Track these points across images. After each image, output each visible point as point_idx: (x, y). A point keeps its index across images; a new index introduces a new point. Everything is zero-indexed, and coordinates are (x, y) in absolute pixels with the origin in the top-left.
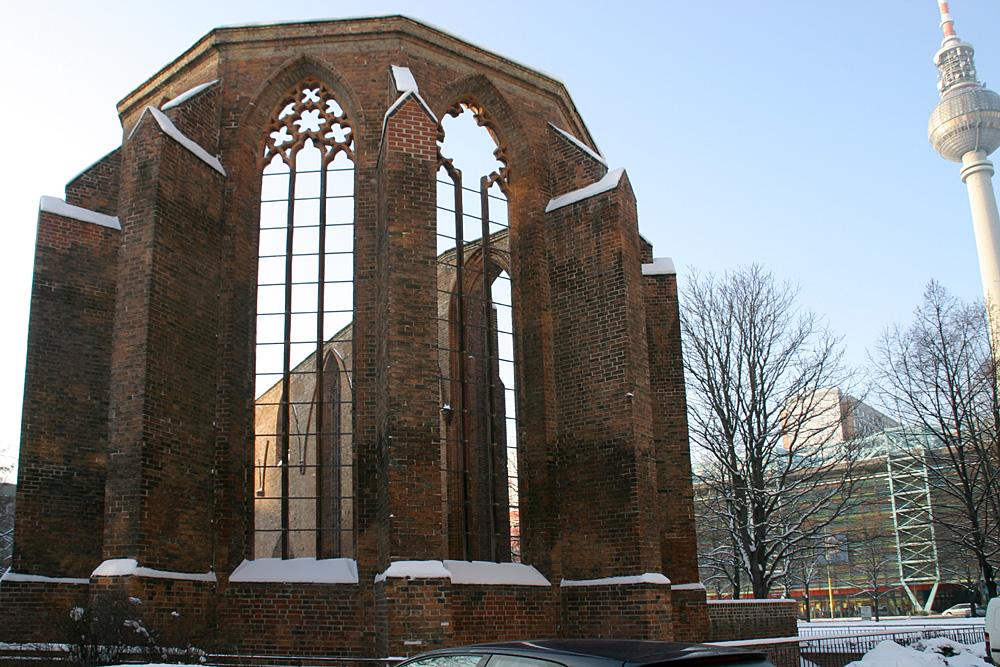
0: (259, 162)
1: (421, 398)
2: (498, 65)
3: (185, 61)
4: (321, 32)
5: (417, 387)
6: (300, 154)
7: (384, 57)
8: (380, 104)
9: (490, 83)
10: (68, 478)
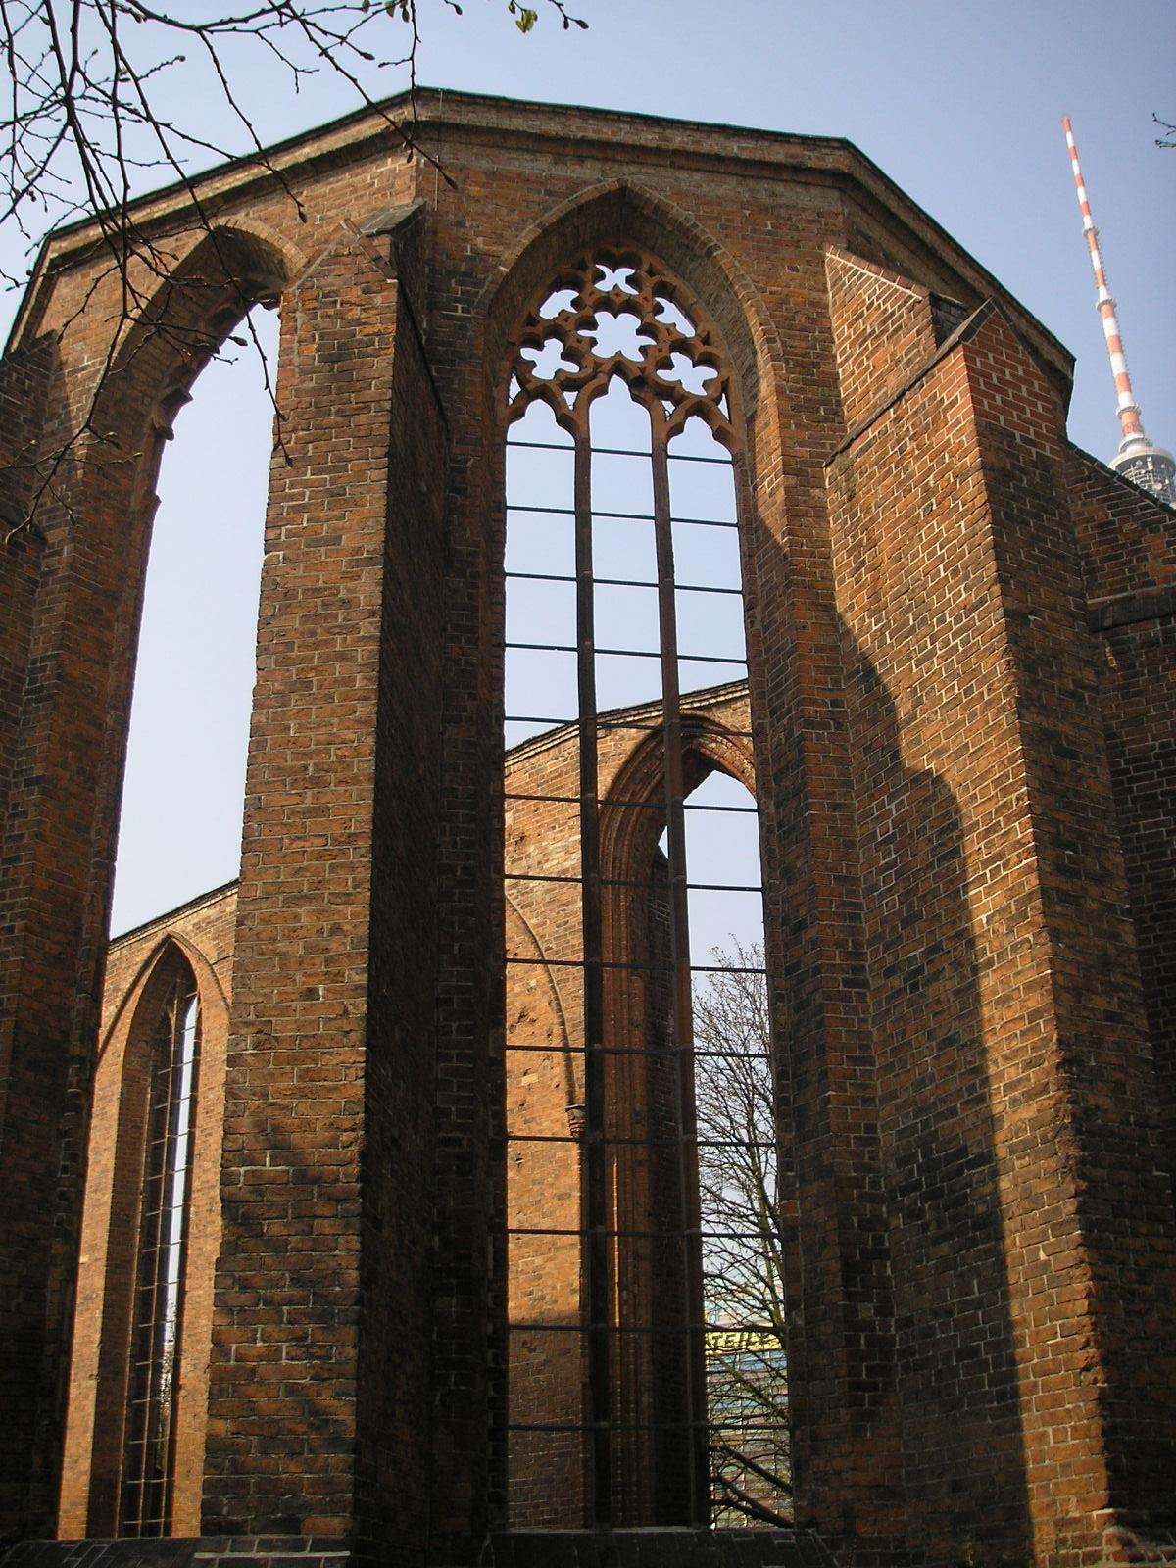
0: (502, 412)
3: (554, 127)
4: (667, 139)
5: (1110, 1017)
6: (597, 405)
7: (809, 222)
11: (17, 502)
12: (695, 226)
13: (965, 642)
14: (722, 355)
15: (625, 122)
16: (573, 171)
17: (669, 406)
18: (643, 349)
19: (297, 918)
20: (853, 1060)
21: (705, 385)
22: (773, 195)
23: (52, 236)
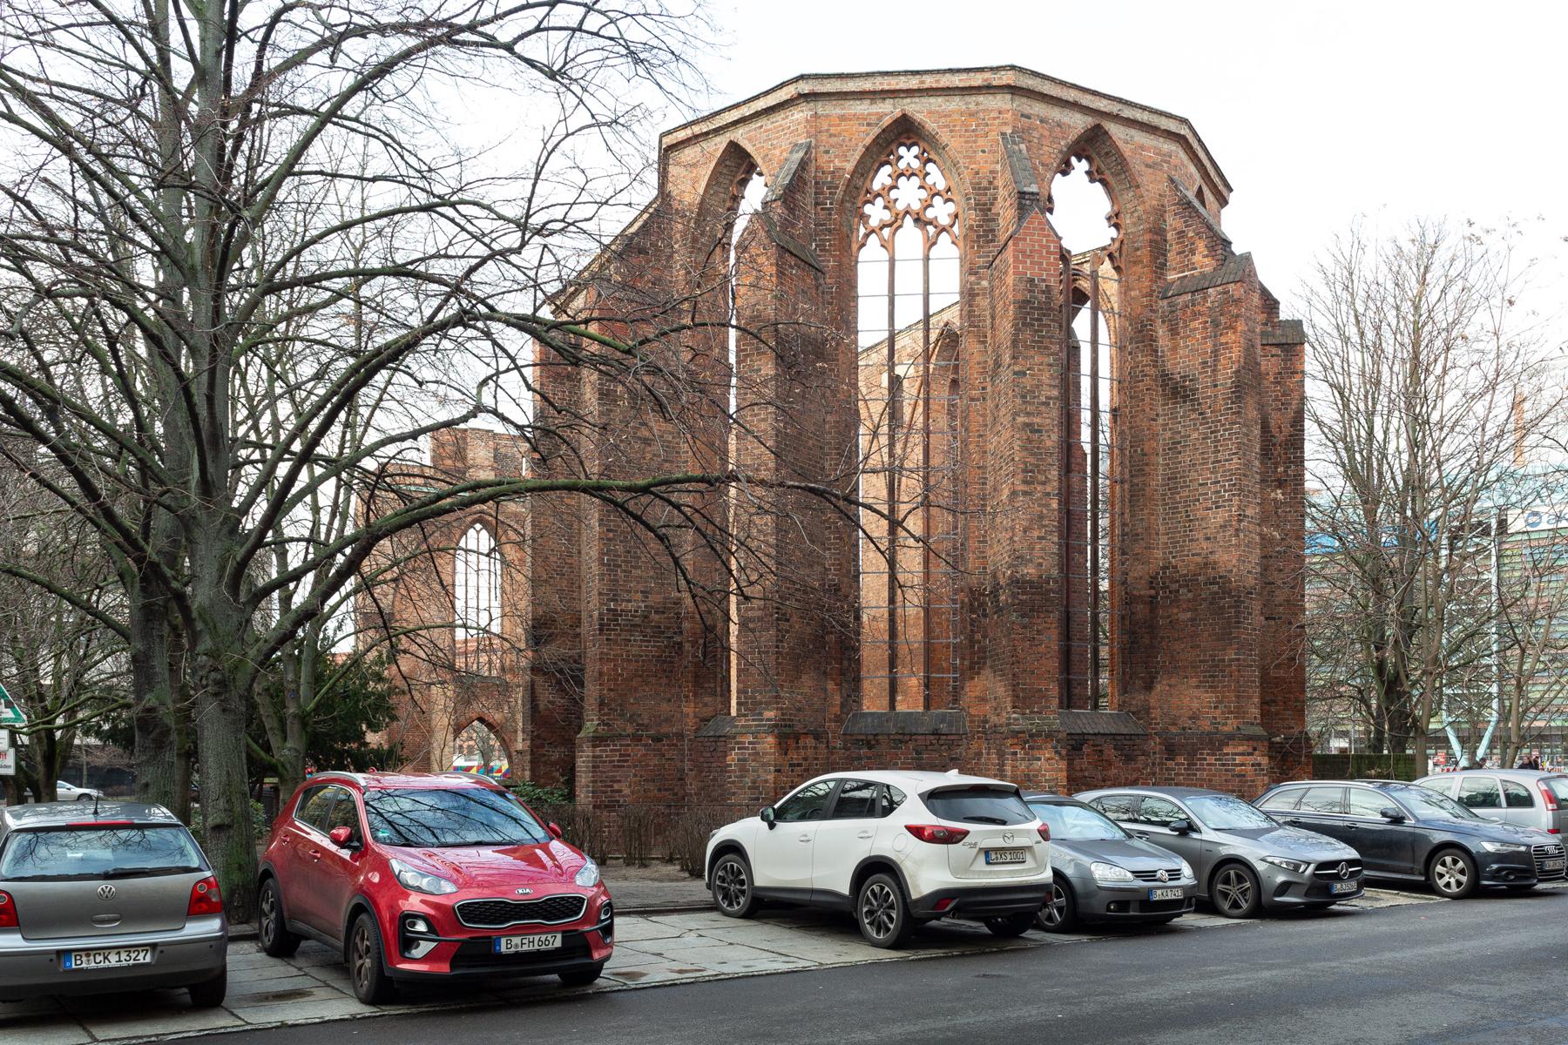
1: (1042, 549)
2: (1114, 108)
5: (1039, 538)
7: (994, 119)
8: (990, 183)
9: (1106, 133)
10: (646, 617)
20: (980, 542)
22: (977, 104)
23: (662, 135)
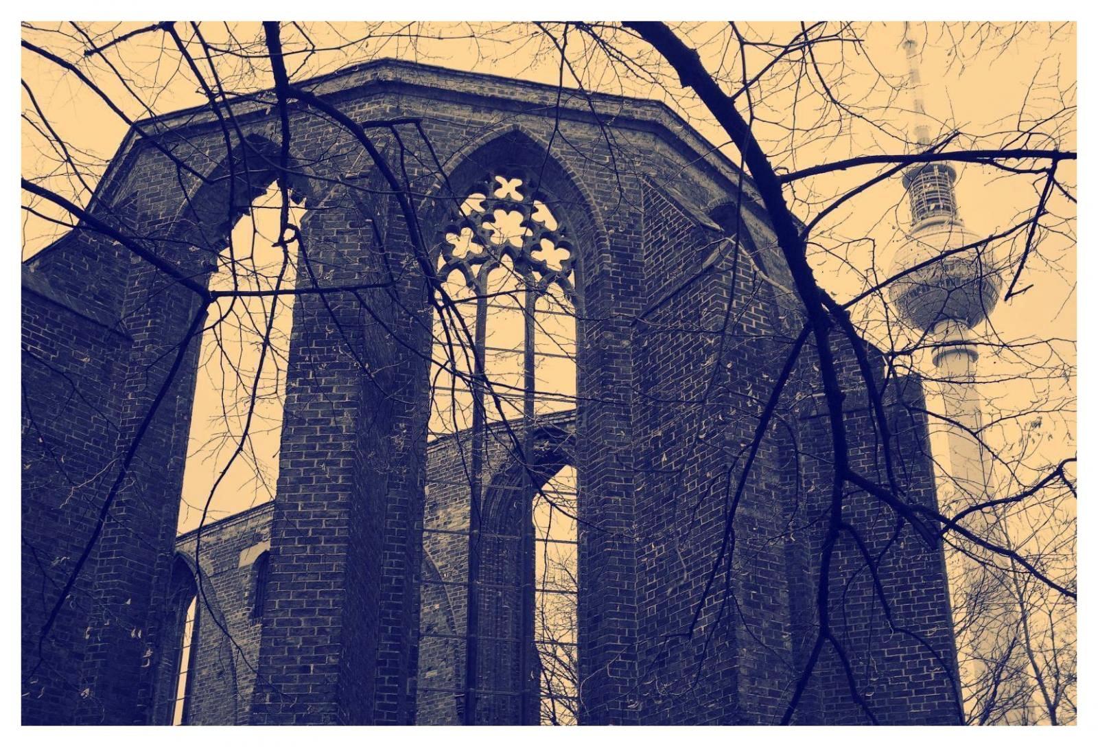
3: (474, 88)
4: (546, 98)
8: (631, 226)
11: (113, 312)
12: (560, 159)
13: (703, 456)
14: (572, 243)
15: (520, 86)
16: (485, 118)
17: (537, 276)
18: (524, 238)
19: (299, 623)
21: (562, 262)
